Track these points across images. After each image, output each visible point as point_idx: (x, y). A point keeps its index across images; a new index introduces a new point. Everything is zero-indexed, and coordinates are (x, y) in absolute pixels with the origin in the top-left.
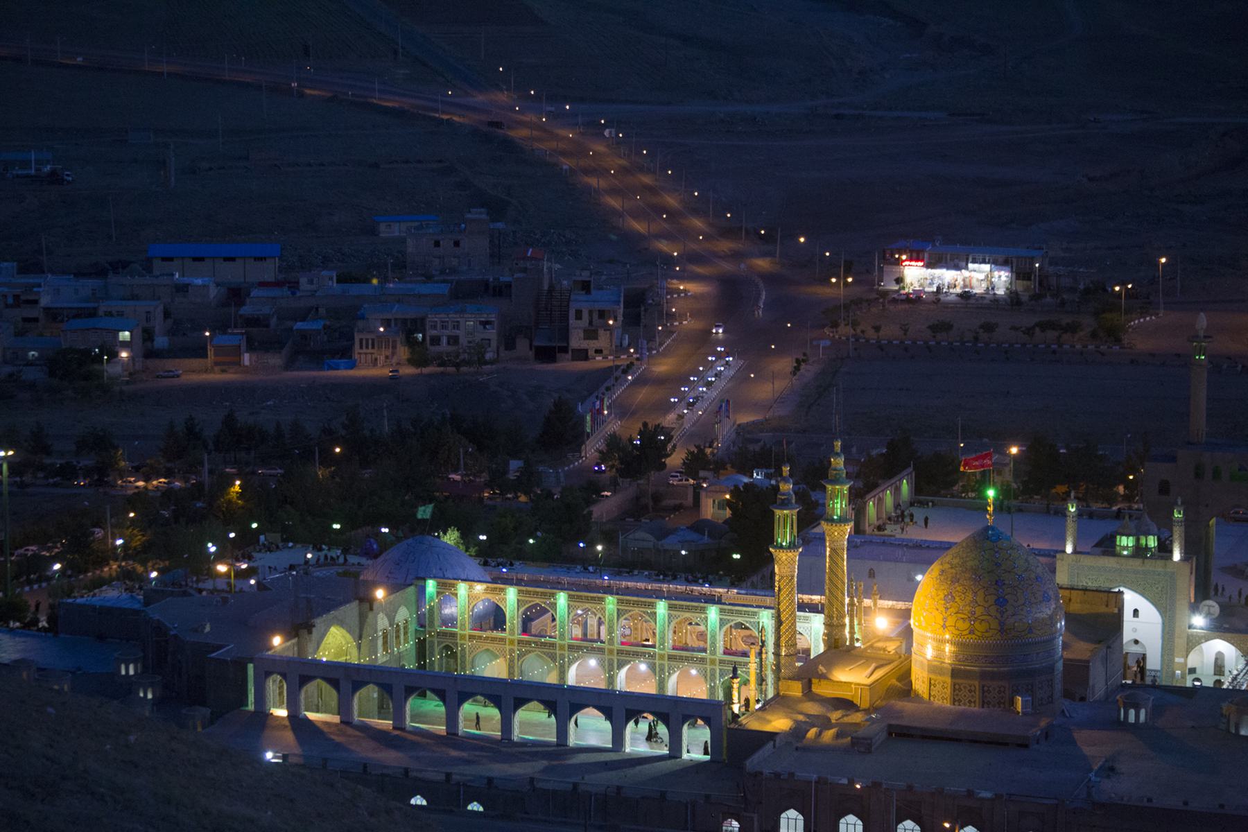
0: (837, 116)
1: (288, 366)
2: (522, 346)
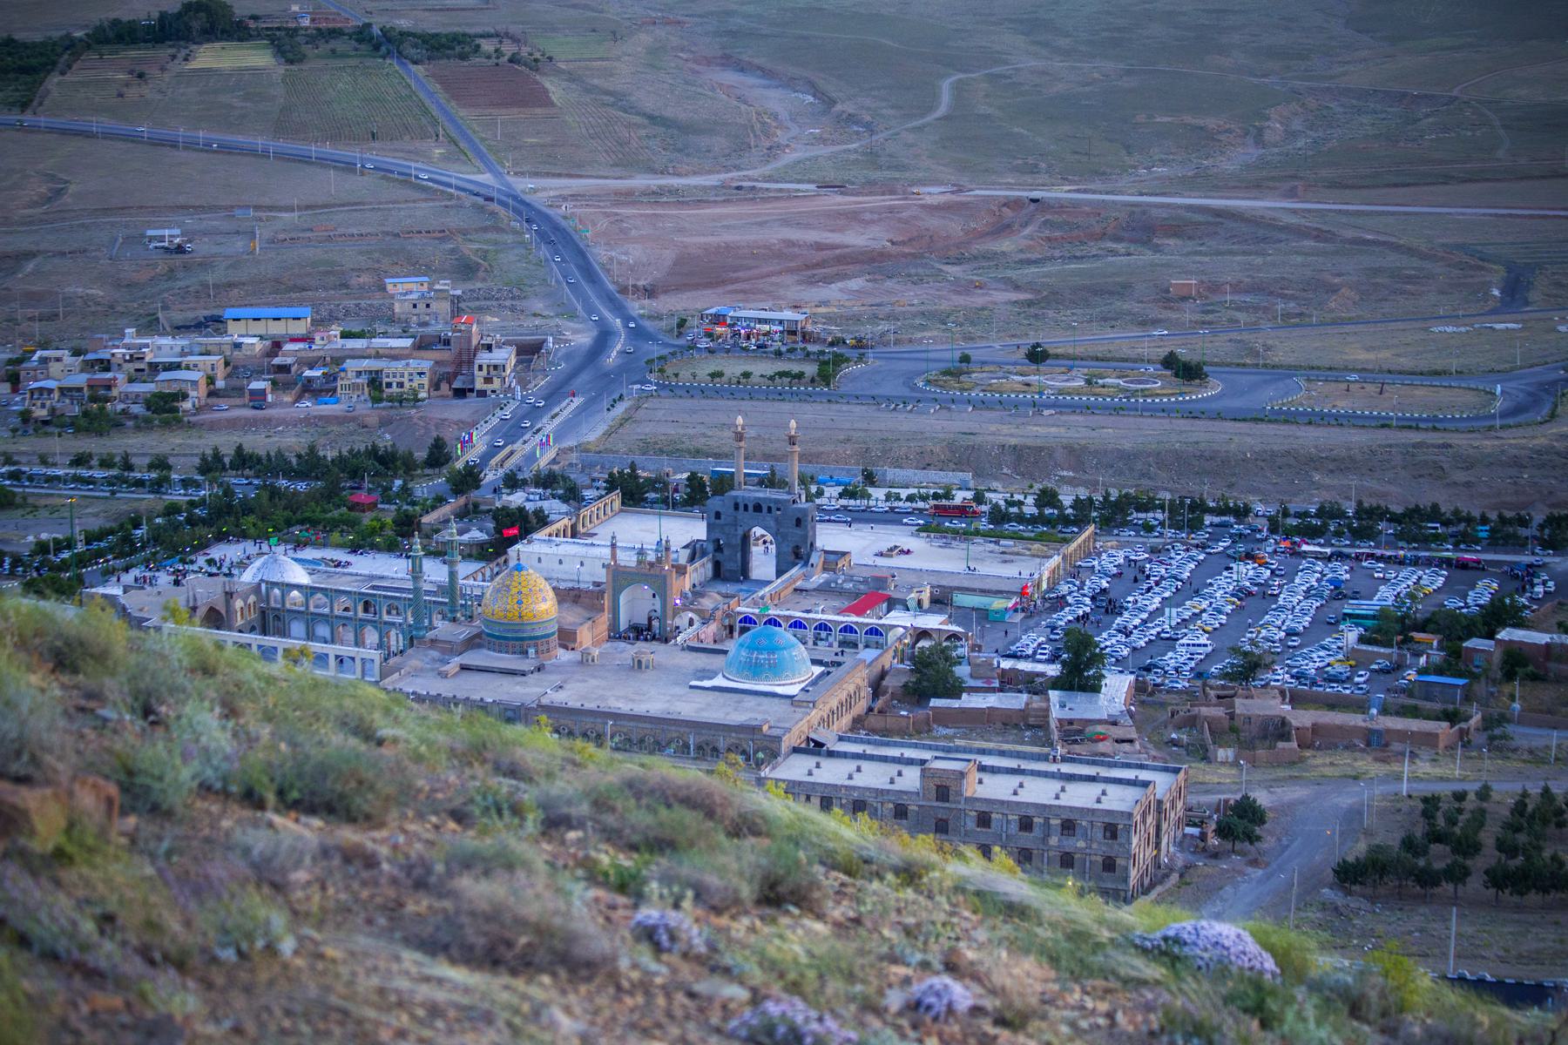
0: (739, 188)
2: (444, 387)
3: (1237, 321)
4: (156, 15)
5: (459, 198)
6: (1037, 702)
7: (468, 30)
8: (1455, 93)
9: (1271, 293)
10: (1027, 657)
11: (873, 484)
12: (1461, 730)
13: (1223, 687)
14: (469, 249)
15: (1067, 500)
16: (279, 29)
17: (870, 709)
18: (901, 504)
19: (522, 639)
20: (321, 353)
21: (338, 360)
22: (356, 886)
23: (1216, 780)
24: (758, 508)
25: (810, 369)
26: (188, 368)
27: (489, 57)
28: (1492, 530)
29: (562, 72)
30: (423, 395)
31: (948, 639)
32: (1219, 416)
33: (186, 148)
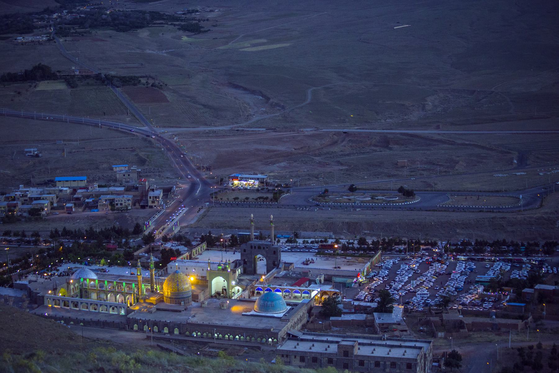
0: (237, 130)
1: (83, 211)
2: (137, 205)
3: (423, 175)
4: (24, 71)
5: (137, 136)
6: (370, 317)
7: (136, 75)
8: (493, 90)
9: (434, 164)
10: (362, 300)
11: (297, 238)
12: (526, 322)
13: (437, 310)
14: (142, 154)
15: (370, 242)
16: (68, 75)
17: (308, 321)
18: (308, 245)
19: (179, 298)
20: (91, 193)
21: (98, 195)
23: (439, 344)
24: (259, 248)
25: (270, 196)
26: (43, 199)
27: (144, 85)
28: (526, 248)
29: (171, 89)
30: (129, 208)
31: (334, 294)
32: (420, 209)
33: (37, 119)
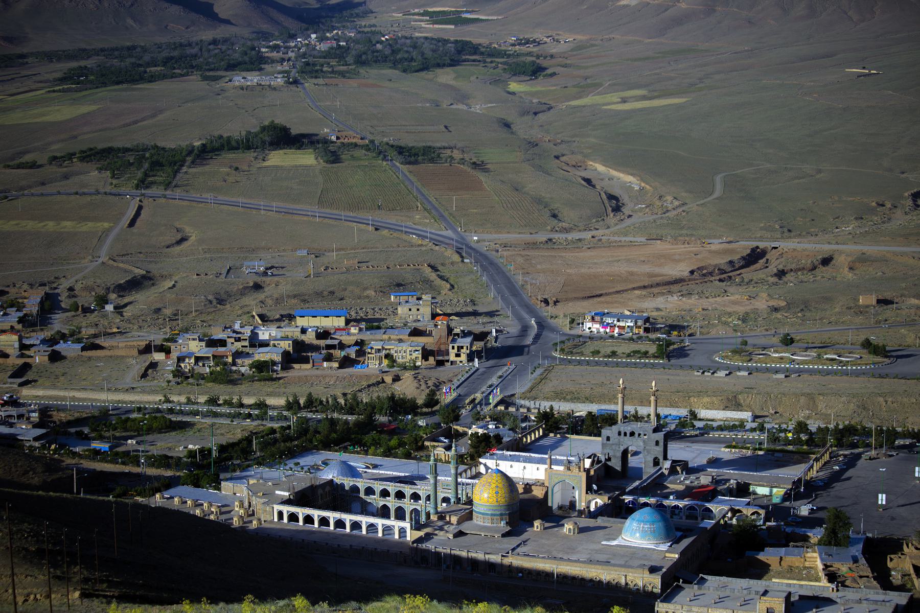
4: (244, 133)
22: (152, 151)
